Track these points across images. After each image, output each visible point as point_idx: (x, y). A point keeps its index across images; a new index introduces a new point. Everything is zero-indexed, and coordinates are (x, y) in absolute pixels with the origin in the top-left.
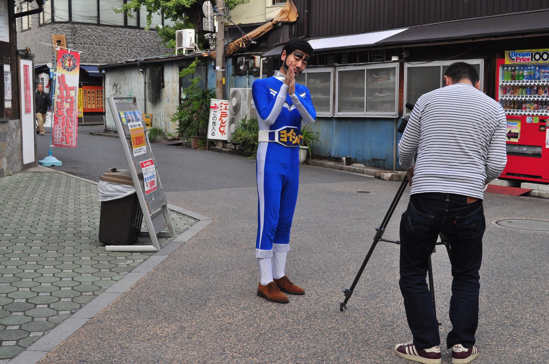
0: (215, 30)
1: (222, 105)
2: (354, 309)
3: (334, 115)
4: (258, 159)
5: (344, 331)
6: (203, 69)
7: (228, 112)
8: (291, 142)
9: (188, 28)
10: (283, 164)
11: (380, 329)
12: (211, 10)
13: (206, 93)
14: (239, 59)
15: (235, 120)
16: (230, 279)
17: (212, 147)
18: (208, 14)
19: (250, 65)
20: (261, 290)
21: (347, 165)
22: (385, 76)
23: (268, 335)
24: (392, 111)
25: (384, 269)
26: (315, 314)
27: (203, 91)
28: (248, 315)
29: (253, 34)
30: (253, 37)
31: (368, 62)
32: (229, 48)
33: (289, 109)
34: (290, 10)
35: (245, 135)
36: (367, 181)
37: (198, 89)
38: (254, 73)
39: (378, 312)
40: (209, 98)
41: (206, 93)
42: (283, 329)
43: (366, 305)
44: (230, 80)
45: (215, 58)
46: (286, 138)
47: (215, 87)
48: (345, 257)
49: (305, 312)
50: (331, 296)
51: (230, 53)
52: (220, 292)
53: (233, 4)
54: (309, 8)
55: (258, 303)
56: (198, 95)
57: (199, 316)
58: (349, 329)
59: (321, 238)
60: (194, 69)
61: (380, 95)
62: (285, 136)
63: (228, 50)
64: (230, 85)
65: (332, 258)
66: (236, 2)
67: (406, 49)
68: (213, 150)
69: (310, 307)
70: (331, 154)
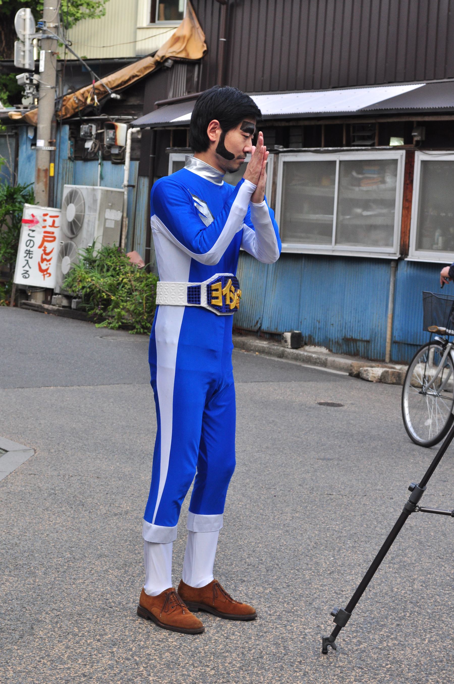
0: (37, 67)
1: (47, 218)
6: (11, 144)
7: (57, 232)
12: (31, 26)
13: (15, 193)
14: (84, 128)
15: (71, 249)
16: (79, 578)
17: (23, 301)
18: (24, 35)
19: (107, 140)
20: (145, 605)
21: (293, 348)
22: (375, 176)
25: (390, 567)
26: (260, 660)
27: (8, 188)
28: (123, 658)
29: (114, 79)
30: (115, 85)
32: (64, 105)
34: (191, 35)
36: (335, 381)
38: (113, 158)
39: (387, 657)
40: (20, 203)
41: (15, 193)
43: (360, 643)
44: (63, 168)
45: (37, 124)
46: (221, 298)
47: (33, 180)
48: (309, 538)
49: (238, 655)
50: (288, 621)
51: (66, 115)
52: (61, 605)
53: (73, 18)
54: (229, 34)
55: (140, 633)
57: (21, 657)
59: (255, 496)
61: (365, 213)
63: (63, 108)
64: (63, 179)
66: (78, 15)
67: (420, 124)
68: (24, 306)
69: (247, 642)
70: (261, 324)
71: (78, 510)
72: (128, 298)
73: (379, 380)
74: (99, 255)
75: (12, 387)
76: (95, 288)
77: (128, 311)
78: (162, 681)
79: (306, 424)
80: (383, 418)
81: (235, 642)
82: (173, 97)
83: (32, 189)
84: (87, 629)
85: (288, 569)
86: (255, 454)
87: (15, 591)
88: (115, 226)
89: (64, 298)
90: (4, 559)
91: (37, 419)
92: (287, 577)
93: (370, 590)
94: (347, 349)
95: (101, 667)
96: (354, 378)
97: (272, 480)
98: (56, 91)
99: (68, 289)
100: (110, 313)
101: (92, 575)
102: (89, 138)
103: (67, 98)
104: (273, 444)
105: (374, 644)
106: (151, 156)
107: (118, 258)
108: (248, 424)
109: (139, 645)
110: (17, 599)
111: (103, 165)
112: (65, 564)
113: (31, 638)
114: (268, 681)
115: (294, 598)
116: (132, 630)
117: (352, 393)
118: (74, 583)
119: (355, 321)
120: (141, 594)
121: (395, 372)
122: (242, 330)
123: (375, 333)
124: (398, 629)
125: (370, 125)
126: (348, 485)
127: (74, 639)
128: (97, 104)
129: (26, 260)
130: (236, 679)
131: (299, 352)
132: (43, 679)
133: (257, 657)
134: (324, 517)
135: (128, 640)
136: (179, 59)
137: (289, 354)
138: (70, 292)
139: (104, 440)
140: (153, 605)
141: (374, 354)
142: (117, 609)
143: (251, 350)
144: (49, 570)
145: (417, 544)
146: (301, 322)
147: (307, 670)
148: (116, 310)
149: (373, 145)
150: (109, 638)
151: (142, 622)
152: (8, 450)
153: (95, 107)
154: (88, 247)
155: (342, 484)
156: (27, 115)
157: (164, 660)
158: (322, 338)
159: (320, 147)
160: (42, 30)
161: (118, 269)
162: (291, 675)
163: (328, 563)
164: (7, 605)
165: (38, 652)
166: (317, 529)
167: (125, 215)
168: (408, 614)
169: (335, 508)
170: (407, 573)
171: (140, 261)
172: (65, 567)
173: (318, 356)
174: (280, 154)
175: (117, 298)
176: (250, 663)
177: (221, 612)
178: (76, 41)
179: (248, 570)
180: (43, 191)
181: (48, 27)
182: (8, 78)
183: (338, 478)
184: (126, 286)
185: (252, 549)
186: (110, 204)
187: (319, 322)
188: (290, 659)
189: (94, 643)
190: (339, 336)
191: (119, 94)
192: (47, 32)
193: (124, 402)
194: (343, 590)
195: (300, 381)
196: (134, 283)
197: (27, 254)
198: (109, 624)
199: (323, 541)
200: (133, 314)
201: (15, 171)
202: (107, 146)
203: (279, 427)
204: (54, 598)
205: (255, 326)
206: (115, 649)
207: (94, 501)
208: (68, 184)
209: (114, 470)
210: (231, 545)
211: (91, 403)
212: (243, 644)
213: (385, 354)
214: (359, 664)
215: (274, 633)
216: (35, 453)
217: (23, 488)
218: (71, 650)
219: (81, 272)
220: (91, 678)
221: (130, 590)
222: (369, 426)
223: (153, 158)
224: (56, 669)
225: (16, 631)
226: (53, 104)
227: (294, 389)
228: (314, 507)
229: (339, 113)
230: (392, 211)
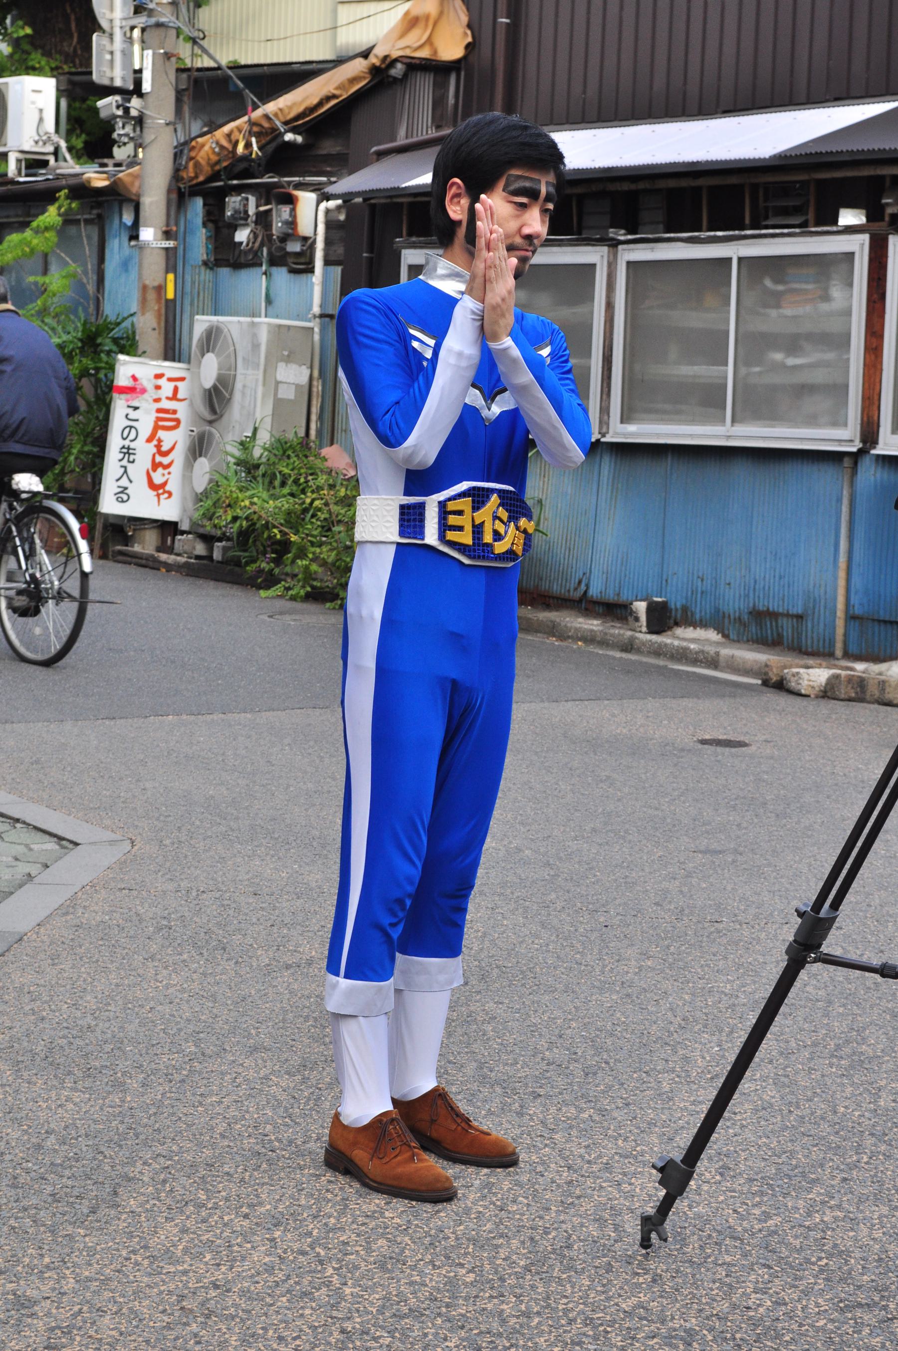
0: (138, 83)
1: (162, 382)
2: (720, 1233)
3: (604, 436)
4: (351, 609)
5: (688, 1325)
6: (89, 238)
7: (182, 410)
8: (487, 545)
9: (28, 74)
10: (456, 637)
11: (833, 1321)
13: (98, 334)
14: (233, 202)
15: (210, 443)
16: (211, 1094)
17: (119, 548)
18: (111, 21)
19: (277, 226)
20: (341, 1145)
21: (651, 631)
22: (810, 287)
23: (375, 1339)
24: (835, 424)
25: (831, 1065)
26: (566, 1252)
27: (85, 324)
29: (289, 103)
31: (743, 229)
32: (192, 159)
33: (485, 413)
34: (441, 13)
35: (252, 504)
36: (735, 696)
37: (67, 316)
38: (290, 260)
39: (820, 1243)
40: (109, 353)
41: (98, 334)
42: (439, 1315)
43: (767, 1216)
44: (193, 283)
46: (468, 528)
47: (134, 308)
49: (523, 1242)
50: (625, 1174)
51: (196, 177)
56: (65, 337)
58: (707, 1318)
59: (567, 927)
60: (51, 235)
61: (791, 361)
62: (465, 521)
63: (191, 164)
64: (192, 304)
65: (618, 1015)
68: (120, 558)
69: (541, 1218)
70: (587, 586)
71: (215, 957)
72: (324, 539)
73: (821, 694)
74: (266, 453)
75: (92, 717)
76: (258, 520)
77: (324, 564)
78: (370, 1295)
79: (674, 782)
80: (828, 768)
81: (518, 1216)
82: (407, 138)
83: (133, 325)
84: (224, 1194)
85: (628, 1070)
86: (570, 843)
87: (83, 1119)
88: (295, 396)
89: (198, 540)
90: (64, 1058)
91: (138, 781)
92: (625, 1086)
93: (790, 1111)
94: (759, 632)
95: (250, 1269)
96: (772, 690)
97: (600, 894)
98: (175, 130)
99: (207, 523)
100: (288, 569)
101: (237, 1087)
102: (242, 222)
103: (197, 142)
104: (606, 824)
105: (796, 1218)
106: (365, 255)
107: (304, 459)
108: (557, 784)
109: (326, 1224)
110: (87, 1136)
111: (270, 275)
112: (184, 1066)
113: (113, 1212)
114: (580, 1294)
115: (639, 1128)
116: (312, 1195)
117: (768, 720)
118: (201, 1104)
119: (774, 577)
120: (333, 1123)
121: (853, 676)
122: (549, 597)
123: (815, 601)
124: (843, 1187)
125: (798, 185)
126: (753, 902)
127: (198, 1213)
128: (257, 153)
129: (122, 466)
130: (517, 1291)
131: (664, 639)
132: (134, 1293)
133: (561, 1247)
134: (702, 966)
135: (305, 1215)
136: (418, 62)
137: (643, 644)
138: (208, 528)
139: (271, 820)
140: (355, 1144)
141: (813, 643)
142: (284, 1153)
143: (569, 637)
144: (152, 1077)
145: (888, 1017)
146: (666, 581)
147: (659, 1271)
148: (299, 562)
149: (804, 225)
150: (267, 1210)
151: (333, 1179)
152: (78, 841)
153: (253, 160)
154: (244, 439)
155: (740, 901)
156: (119, 179)
157: (374, 1254)
158: (708, 612)
159: (700, 230)
160: (145, 9)
161: (302, 480)
162: (627, 1282)
163: (708, 1058)
164: (67, 1147)
165: (125, 1240)
166: (689, 991)
167: (316, 373)
168: (865, 1157)
169: (726, 949)
170: (866, 1076)
171: (347, 464)
172: (184, 1072)
173: (701, 647)
174: (620, 247)
175: (303, 539)
176: (546, 1258)
177: (447, 1149)
178: (212, 32)
179: (548, 1075)
180: (154, 329)
181: (157, 4)
182: (84, 106)
183: (733, 889)
184: (319, 513)
185: (557, 1032)
186: (286, 353)
187: (702, 580)
188: (627, 1250)
189: (236, 1221)
190: (742, 607)
191: (299, 134)
192: (156, 13)
193: (311, 743)
194: (737, 1111)
195: (664, 697)
196: (335, 508)
197: (125, 453)
198: (267, 1184)
199: (698, 1014)
200: (333, 569)
201: (98, 291)
202: (278, 237)
203: (620, 790)
204: (160, 1132)
205: (576, 589)
206: (277, 1234)
207: (246, 941)
208: (203, 314)
209: (289, 878)
210: (515, 1024)
211: (247, 747)
212: (534, 1220)
213: (834, 642)
214: (765, 1258)
215: (596, 1197)
216: (133, 847)
217: (107, 917)
218: (191, 1236)
219: (231, 487)
220: (228, 1291)
221: (311, 1115)
222: (799, 786)
223: (370, 260)
224: (161, 1273)
225: (83, 1198)
226: (171, 156)
227: (650, 714)
228: (683, 948)
229: (736, 161)
230: (846, 357)
